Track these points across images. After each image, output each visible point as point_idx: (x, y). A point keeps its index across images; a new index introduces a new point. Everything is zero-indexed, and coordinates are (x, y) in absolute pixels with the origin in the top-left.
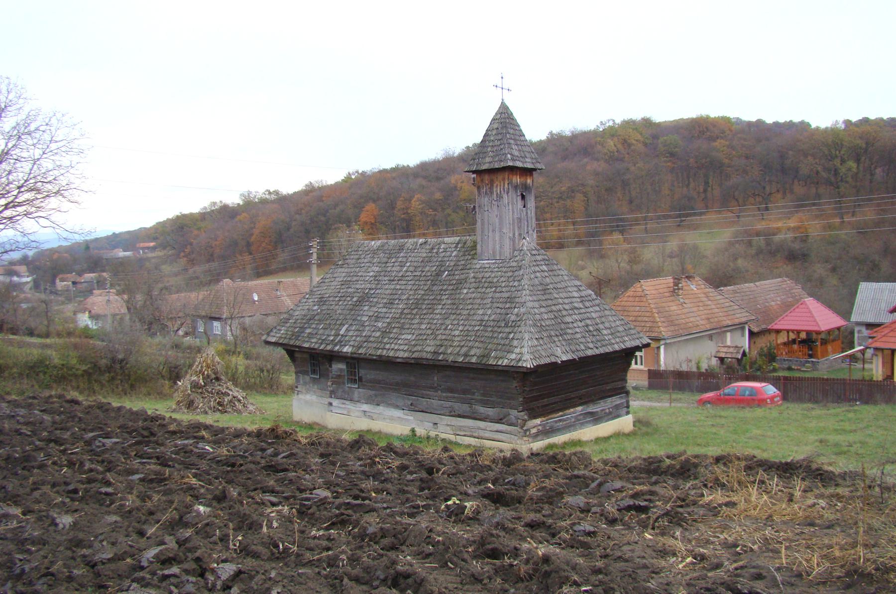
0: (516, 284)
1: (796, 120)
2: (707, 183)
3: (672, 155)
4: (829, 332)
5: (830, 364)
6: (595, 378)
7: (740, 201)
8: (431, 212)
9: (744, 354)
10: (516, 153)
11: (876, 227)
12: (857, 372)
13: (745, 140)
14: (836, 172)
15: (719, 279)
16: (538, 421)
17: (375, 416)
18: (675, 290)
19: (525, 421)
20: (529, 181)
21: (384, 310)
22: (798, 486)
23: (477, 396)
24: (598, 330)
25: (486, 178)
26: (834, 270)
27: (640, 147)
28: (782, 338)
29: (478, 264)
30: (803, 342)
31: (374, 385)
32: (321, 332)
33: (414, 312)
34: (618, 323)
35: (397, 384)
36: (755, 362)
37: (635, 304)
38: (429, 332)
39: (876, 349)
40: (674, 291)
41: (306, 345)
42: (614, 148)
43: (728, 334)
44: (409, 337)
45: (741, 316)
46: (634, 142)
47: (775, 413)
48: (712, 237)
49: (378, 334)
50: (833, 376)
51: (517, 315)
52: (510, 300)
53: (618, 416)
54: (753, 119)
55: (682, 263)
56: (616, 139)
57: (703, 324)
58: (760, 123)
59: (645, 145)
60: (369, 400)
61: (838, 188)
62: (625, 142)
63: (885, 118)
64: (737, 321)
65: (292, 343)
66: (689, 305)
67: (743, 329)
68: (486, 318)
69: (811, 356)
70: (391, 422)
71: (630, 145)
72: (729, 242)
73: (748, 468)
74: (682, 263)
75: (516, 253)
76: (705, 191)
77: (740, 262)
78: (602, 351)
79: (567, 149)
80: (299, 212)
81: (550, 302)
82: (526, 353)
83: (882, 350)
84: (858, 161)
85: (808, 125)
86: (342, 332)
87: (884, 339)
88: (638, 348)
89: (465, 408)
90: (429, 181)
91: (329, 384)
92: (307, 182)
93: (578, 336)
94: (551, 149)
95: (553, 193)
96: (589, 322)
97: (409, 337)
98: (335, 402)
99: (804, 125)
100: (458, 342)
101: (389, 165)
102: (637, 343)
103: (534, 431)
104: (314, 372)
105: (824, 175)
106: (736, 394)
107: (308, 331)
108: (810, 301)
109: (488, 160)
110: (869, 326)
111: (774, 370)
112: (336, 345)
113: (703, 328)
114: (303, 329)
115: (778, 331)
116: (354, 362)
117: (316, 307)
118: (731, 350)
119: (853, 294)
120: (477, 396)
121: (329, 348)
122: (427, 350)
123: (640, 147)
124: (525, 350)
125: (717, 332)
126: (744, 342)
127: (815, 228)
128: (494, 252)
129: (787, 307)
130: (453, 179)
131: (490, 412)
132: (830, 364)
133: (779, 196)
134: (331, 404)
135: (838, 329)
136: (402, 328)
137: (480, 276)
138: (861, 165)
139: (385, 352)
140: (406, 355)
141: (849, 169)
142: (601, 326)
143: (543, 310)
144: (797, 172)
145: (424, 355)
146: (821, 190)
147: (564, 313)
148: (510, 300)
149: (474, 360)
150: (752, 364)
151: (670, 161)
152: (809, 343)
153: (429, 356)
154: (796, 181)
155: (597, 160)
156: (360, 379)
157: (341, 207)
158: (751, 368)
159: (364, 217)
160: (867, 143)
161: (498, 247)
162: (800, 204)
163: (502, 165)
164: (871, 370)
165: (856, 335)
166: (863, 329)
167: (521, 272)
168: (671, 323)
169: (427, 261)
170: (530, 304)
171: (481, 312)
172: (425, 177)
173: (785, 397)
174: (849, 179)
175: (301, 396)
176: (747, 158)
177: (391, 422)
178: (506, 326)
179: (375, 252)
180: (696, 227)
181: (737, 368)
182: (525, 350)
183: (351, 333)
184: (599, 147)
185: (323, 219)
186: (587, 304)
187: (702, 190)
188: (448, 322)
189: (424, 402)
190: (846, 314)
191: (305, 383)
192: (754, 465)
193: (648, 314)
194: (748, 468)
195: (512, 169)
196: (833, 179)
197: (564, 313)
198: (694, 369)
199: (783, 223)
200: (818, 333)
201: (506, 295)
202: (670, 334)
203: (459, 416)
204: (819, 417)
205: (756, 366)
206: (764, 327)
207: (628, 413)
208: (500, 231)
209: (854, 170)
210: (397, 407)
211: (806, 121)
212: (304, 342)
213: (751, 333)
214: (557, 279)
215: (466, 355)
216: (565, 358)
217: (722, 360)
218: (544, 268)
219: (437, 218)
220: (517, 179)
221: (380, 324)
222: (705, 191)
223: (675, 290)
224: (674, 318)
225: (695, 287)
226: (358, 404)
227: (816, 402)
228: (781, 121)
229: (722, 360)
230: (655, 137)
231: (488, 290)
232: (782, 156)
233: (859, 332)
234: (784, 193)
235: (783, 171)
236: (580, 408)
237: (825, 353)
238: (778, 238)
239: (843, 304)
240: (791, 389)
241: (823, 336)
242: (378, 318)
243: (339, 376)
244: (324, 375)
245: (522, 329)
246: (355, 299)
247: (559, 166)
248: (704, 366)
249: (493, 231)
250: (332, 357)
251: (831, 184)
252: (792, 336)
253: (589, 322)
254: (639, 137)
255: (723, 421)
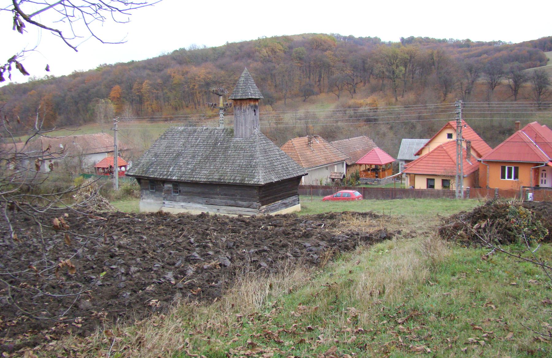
0: (253, 149)
1: (372, 36)
2: (320, 76)
3: (301, 59)
4: (386, 165)
5: (386, 181)
6: (289, 187)
7: (340, 87)
8: (155, 91)
9: (344, 177)
10: (252, 92)
11: (414, 104)
12: (398, 185)
13: (343, 51)
14: (394, 73)
15: (329, 135)
16: (264, 207)
17: (188, 208)
18: (309, 144)
19: (260, 206)
20: (257, 104)
21: (191, 160)
22: (368, 218)
23: (238, 197)
24: (287, 168)
25: (239, 102)
26: (391, 128)
27: (281, 54)
28: (363, 168)
29: (235, 140)
30: (373, 170)
31: (187, 193)
32: (159, 170)
33: (206, 161)
34: (295, 165)
35: (199, 193)
36: (349, 180)
37: (289, 151)
38: (215, 170)
39: (407, 174)
40: (308, 144)
41: (152, 176)
42: (266, 54)
43: (336, 166)
44: (206, 172)
45: (342, 157)
46: (278, 51)
47: (360, 203)
48: (323, 109)
49: (189, 171)
50: (388, 187)
51: (255, 162)
52: (252, 156)
53: (295, 205)
54: (347, 35)
55: (307, 123)
56: (267, 48)
57: (323, 161)
58: (351, 38)
59: (285, 52)
60: (184, 201)
61: (394, 81)
62: (273, 51)
63: (423, 37)
64: (340, 160)
65: (143, 175)
66: (316, 152)
67: (343, 163)
68: (241, 164)
69: (377, 177)
70: (195, 209)
71: (275, 52)
72: (333, 111)
73: (352, 215)
74: (307, 123)
75: (252, 135)
76: (319, 81)
77: (339, 124)
78: (289, 177)
79: (238, 54)
80: (70, 90)
81: (268, 157)
82: (261, 178)
83: (410, 174)
84: (406, 66)
85: (379, 40)
86: (171, 170)
87: (410, 169)
88: (303, 175)
89: (232, 202)
90: (153, 71)
91: (163, 194)
92: (73, 71)
93: (280, 171)
94: (228, 53)
95: (230, 81)
96: (283, 165)
97: (206, 172)
98: (167, 202)
99: (376, 41)
100: (230, 175)
101: (126, 61)
102: (303, 173)
103: (263, 211)
104: (152, 189)
105: (387, 74)
106: (342, 196)
107: (151, 170)
108: (377, 149)
109: (239, 95)
110: (407, 161)
111: (359, 184)
112: (168, 176)
113: (323, 163)
114: (148, 169)
115: (361, 165)
116: (177, 184)
117: (153, 159)
118: (338, 174)
119: (400, 143)
120: (238, 197)
121: (165, 177)
122: (215, 177)
123: (281, 54)
124: (260, 177)
125: (330, 165)
126: (344, 170)
127: (381, 105)
128: (242, 134)
129: (366, 151)
130: (169, 71)
131: (245, 203)
132: (386, 181)
133: (362, 84)
134: (164, 203)
135: (391, 163)
136: (201, 168)
137: (236, 145)
138: (407, 68)
139: (194, 179)
140: (205, 180)
141: (401, 71)
142: (288, 167)
143: (266, 160)
144: (372, 71)
145: (214, 180)
146: (385, 82)
147: (274, 161)
148: (252, 156)
149: (238, 182)
150: (348, 181)
151: (299, 63)
152: (376, 170)
153: (217, 180)
154: (371, 77)
155: (256, 61)
156: (180, 191)
157: (98, 87)
158: (347, 183)
159: (112, 94)
160: (411, 57)
161: (244, 133)
162: (373, 90)
163: (247, 97)
164: (404, 184)
165: (400, 166)
166: (404, 163)
167: (255, 144)
168: (307, 161)
169: (209, 137)
170: (260, 158)
171: (238, 161)
172: (150, 69)
173: (364, 197)
174: (401, 76)
175: (144, 200)
176: (344, 62)
177: (195, 209)
178: (251, 167)
179: (181, 132)
180: (313, 102)
181: (340, 183)
182: (260, 177)
183: (175, 171)
184: (257, 53)
185: (86, 95)
186: (282, 157)
187: (317, 80)
188: (223, 165)
189: (212, 200)
190: (394, 155)
191: (147, 194)
192: (353, 214)
193: (296, 157)
194: (352, 215)
195: (250, 99)
196: (392, 76)
197: (274, 161)
198: (319, 185)
199: (364, 101)
200: (381, 165)
201: (250, 154)
202: (307, 167)
203: (230, 206)
204: (378, 204)
205: (350, 182)
206: (353, 162)
207: (299, 203)
208: (245, 125)
209: (403, 72)
210: (199, 203)
211: (378, 37)
212: (150, 175)
213: (347, 165)
214: (269, 147)
215: (234, 180)
216: (276, 180)
217: (333, 179)
218: (264, 142)
219: (159, 94)
220: (252, 103)
221: (190, 167)
222: (319, 81)
223: (309, 144)
224: (309, 158)
225: (319, 142)
226: (179, 203)
227: (378, 199)
228: (364, 36)
229: (333, 179)
230: (291, 48)
231: (241, 152)
232: (364, 62)
233: (401, 164)
234: (365, 83)
235: (364, 70)
236: (280, 201)
237: (384, 176)
238: (361, 110)
239: (393, 151)
240: (366, 193)
241: (384, 166)
242: (188, 164)
243: (168, 190)
244: (160, 190)
245: (259, 168)
246: (174, 155)
247: (233, 64)
248: (324, 183)
249: (242, 125)
250: (165, 181)
251: (391, 78)
252: (368, 167)
253: (283, 165)
254: (281, 48)
255: (337, 207)
